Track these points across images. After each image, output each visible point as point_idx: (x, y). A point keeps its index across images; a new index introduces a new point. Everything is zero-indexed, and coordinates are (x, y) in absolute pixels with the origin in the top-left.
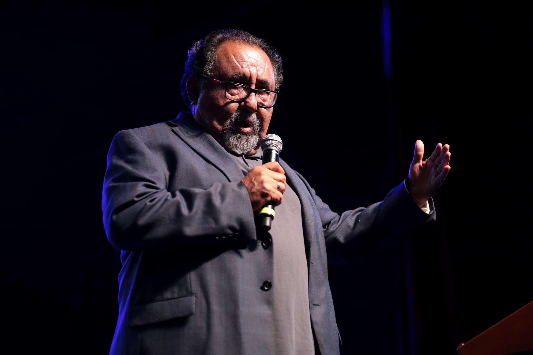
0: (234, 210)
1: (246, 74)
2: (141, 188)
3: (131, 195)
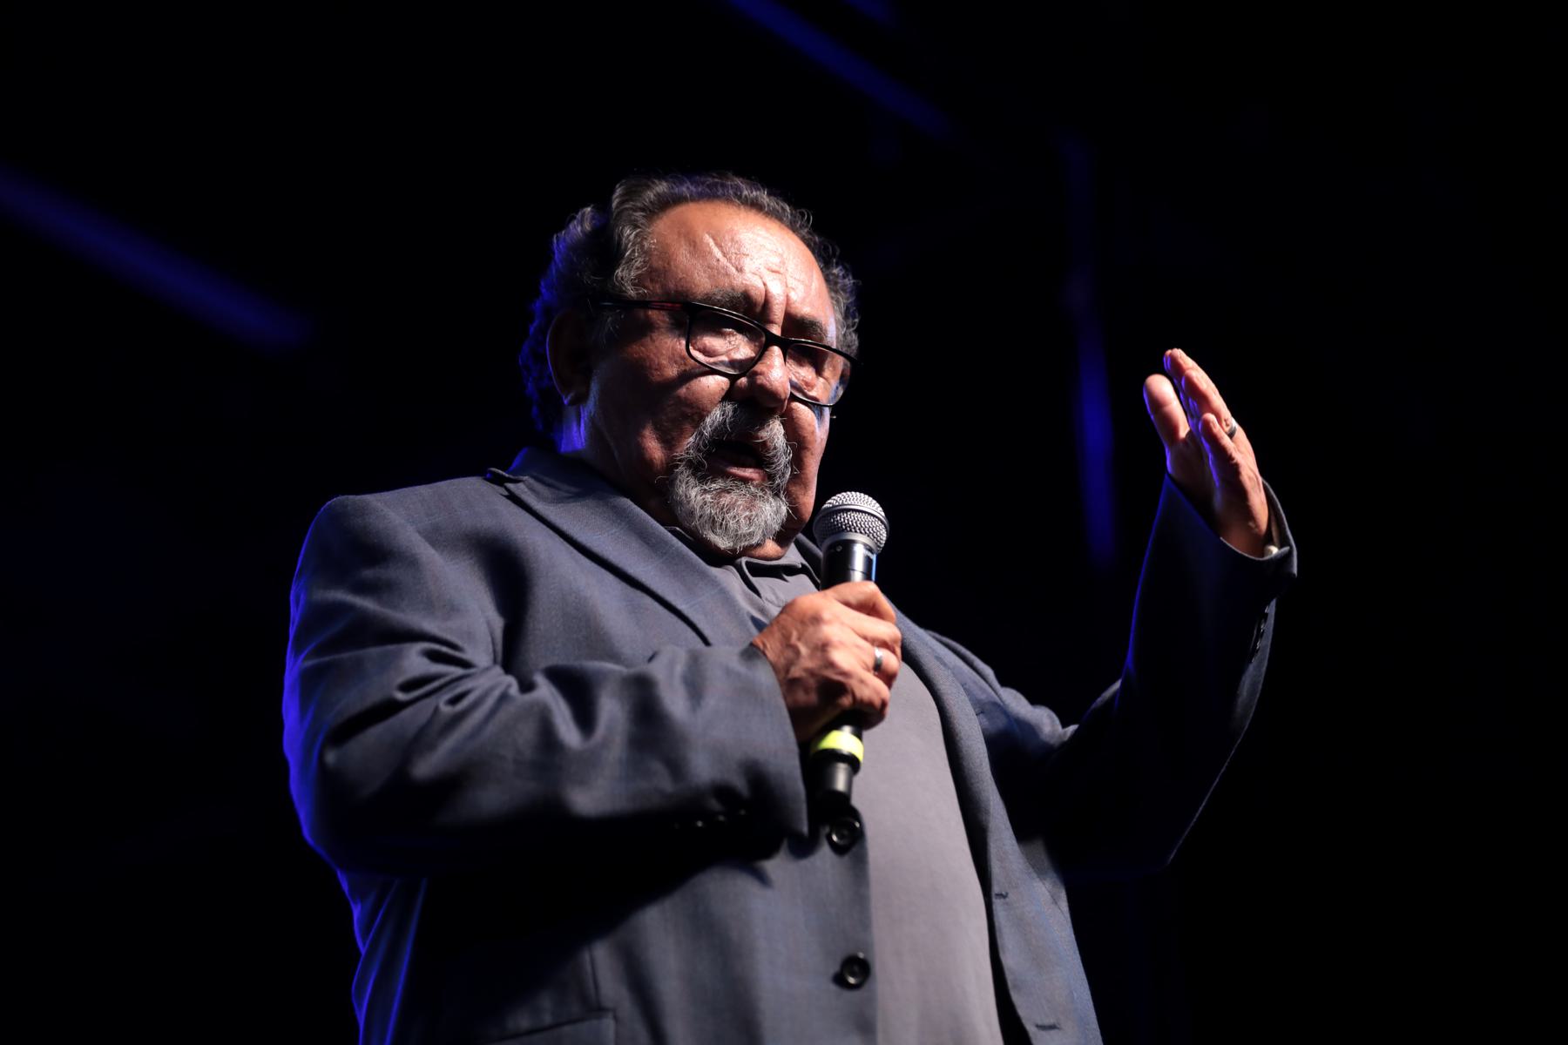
0: (732, 729)
1: (753, 293)
2: (414, 661)
3: (387, 686)
